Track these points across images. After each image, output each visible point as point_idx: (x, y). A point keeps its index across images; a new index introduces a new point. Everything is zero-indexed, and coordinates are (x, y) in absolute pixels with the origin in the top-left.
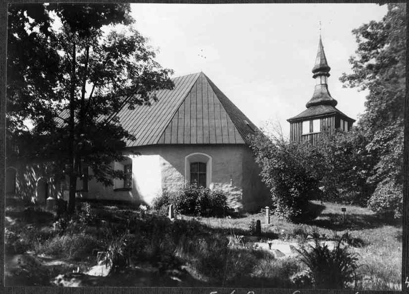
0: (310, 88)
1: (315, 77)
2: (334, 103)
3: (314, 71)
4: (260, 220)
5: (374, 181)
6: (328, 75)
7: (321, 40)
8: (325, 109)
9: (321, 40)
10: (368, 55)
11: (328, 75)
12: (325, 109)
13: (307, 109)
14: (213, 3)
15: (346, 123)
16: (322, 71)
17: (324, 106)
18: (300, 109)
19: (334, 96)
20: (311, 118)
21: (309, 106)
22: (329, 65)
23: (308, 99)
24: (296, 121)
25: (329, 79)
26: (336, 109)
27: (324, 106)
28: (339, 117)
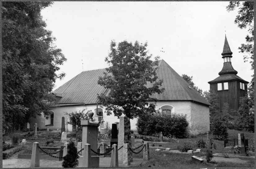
0: (219, 64)
1: (223, 58)
2: (236, 73)
3: (222, 54)
4: (65, 117)
5: (151, 125)
6: (231, 57)
7: (226, 37)
8: (230, 77)
9: (226, 37)
10: (229, 120)
11: (231, 57)
12: (230, 77)
13: (219, 76)
14: (139, 1)
15: (243, 84)
16: (227, 54)
17: (228, 73)
18: (215, 76)
19: (235, 68)
20: (222, 82)
21: (220, 74)
22: (232, 51)
23: (220, 70)
24: (213, 84)
25: (231, 59)
26: (237, 76)
27: (228, 73)
28: (240, 81)
